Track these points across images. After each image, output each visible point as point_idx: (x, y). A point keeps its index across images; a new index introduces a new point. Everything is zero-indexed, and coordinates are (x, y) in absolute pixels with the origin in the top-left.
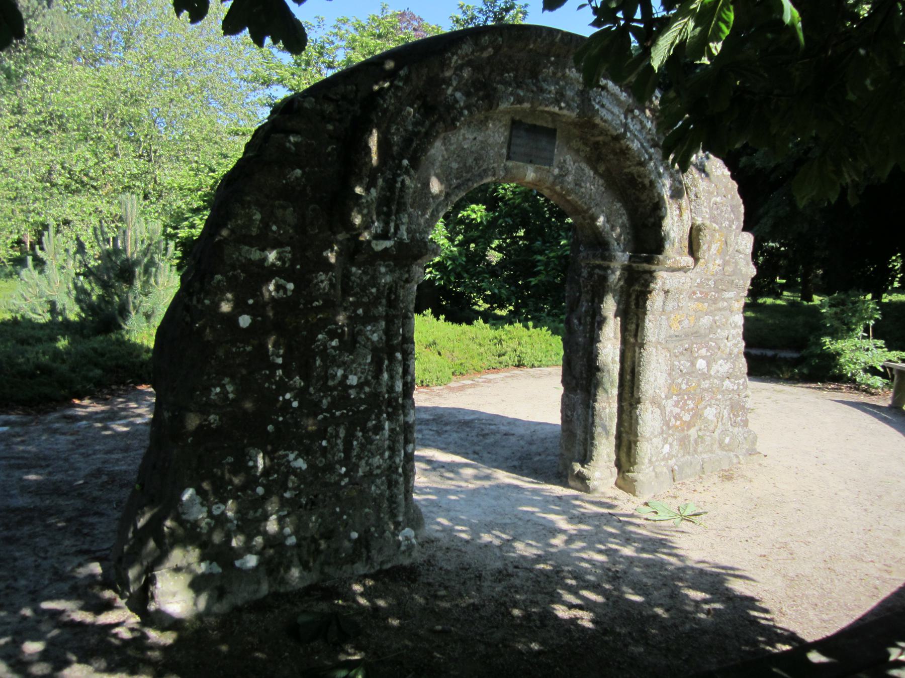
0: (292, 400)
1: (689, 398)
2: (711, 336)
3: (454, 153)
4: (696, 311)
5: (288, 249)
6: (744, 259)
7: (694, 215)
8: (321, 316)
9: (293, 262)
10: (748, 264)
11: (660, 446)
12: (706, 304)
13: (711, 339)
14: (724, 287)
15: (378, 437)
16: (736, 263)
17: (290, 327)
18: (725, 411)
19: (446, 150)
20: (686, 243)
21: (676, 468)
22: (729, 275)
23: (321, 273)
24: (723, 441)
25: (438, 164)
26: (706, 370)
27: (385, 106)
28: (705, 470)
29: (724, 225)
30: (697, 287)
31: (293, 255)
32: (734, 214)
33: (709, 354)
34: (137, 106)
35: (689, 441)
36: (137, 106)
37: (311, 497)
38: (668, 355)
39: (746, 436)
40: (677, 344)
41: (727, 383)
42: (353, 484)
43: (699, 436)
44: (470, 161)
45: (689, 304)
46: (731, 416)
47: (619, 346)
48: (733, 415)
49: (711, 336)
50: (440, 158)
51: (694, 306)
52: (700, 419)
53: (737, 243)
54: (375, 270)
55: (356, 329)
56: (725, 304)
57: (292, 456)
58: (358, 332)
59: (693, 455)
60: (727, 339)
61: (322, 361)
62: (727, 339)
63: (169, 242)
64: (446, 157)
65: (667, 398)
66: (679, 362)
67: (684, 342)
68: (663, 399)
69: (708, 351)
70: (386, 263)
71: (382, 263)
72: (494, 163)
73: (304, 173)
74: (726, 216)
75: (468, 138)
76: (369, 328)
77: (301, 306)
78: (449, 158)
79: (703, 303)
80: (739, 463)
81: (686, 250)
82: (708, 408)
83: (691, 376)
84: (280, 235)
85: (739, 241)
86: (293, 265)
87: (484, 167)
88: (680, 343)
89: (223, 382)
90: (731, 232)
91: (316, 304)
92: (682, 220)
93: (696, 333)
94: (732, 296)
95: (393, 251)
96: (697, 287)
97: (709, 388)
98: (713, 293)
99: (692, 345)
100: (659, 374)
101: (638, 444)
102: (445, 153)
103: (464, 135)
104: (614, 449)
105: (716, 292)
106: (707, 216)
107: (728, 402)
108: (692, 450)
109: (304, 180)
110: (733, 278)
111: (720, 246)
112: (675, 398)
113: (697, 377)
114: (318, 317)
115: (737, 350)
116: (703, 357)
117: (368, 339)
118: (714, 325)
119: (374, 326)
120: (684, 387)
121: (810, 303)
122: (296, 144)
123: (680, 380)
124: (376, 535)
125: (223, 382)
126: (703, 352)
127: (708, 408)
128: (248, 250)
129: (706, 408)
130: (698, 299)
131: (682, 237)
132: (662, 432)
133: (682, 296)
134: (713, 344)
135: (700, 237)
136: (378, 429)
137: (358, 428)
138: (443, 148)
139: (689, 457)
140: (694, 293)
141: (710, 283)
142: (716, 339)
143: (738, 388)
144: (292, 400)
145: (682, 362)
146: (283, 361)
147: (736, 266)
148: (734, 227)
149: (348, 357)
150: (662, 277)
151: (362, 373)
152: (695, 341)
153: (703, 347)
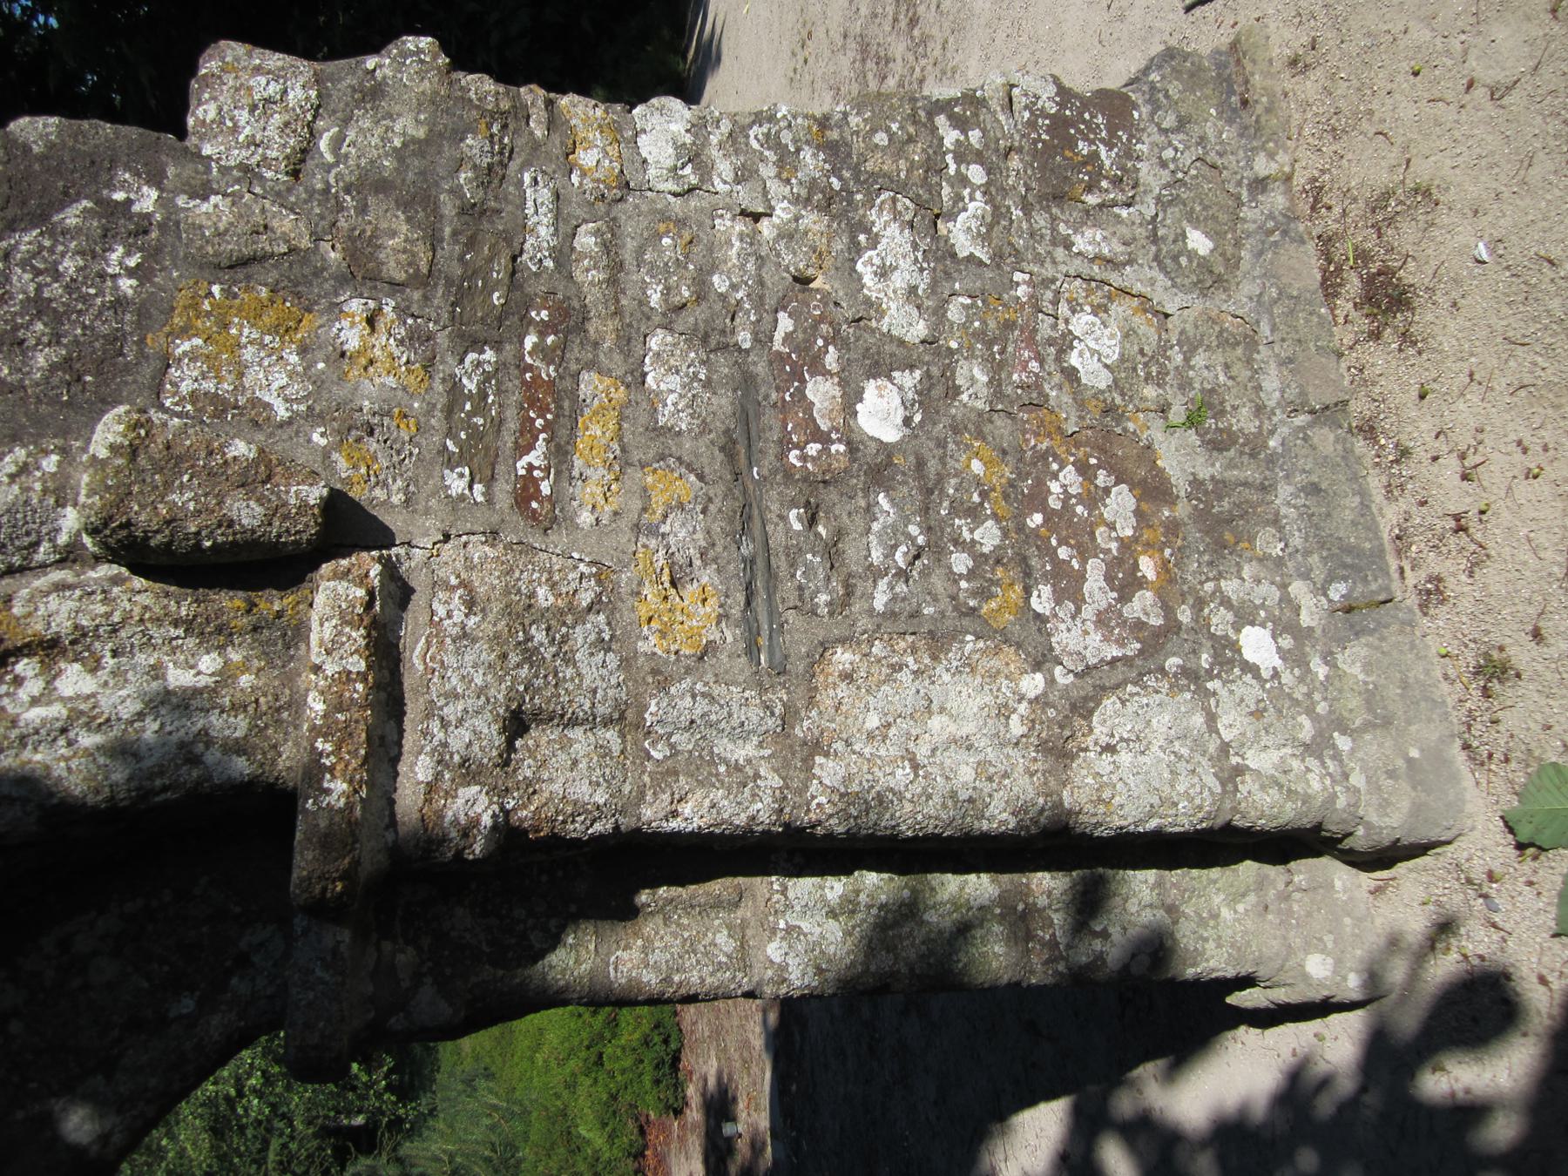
1: (1038, 499)
2: (744, 338)
4: (623, 462)
6: (346, 121)
7: (43, 553)
10: (373, 94)
11: (1249, 689)
12: (590, 384)
13: (763, 338)
14: (498, 273)
16: (369, 184)
18: (1081, 243)
20: (229, 602)
21: (1338, 591)
22: (434, 242)
24: (1204, 264)
26: (909, 380)
28: (1330, 400)
29: (127, 285)
30: (490, 481)
32: (67, 199)
33: (831, 359)
34: (145, 694)
35: (1221, 487)
36: (145, 694)
38: (843, 657)
39: (1169, 121)
40: (787, 590)
41: (962, 234)
43: (1192, 421)
45: (585, 518)
46: (1092, 200)
47: (776, 881)
48: (1089, 189)
49: (744, 338)
51: (598, 474)
52: (1120, 419)
53: (248, 172)
56: (586, 240)
59: (1272, 460)
60: (756, 217)
62: (756, 217)
63: (371, 200)
65: (1042, 660)
66: (876, 574)
67: (777, 538)
68: (1051, 682)
69: (818, 368)
74: (69, 265)
79: (578, 406)
80: (1288, 178)
81: (273, 602)
82: (1074, 359)
83: (941, 479)
85: (238, 156)
88: (780, 563)
90: (172, 223)
92: (80, 634)
93: (729, 450)
94: (545, 194)
96: (490, 481)
97: (988, 360)
98: (530, 341)
99: (788, 473)
100: (936, 723)
104: (1215, 872)
105: (526, 323)
106: (50, 463)
107: (1041, 220)
108: (1250, 473)
110: (448, 207)
111: (255, 317)
112: (1042, 601)
113: (941, 444)
115: (807, 154)
116: (851, 399)
118: (687, 320)
120: (988, 536)
121: (1393, 996)
123: (960, 562)
126: (821, 392)
127: (1074, 359)
129: (1071, 374)
130: (561, 454)
131: (189, 625)
132: (1192, 676)
133: (544, 597)
134: (785, 323)
135: (181, 547)
139: (1284, 491)
140: (526, 490)
141: (470, 385)
142: (759, 303)
143: (979, 158)
145: (877, 555)
147: (382, 186)
148: (147, 200)
150: (431, 788)
152: (769, 460)
153: (800, 394)
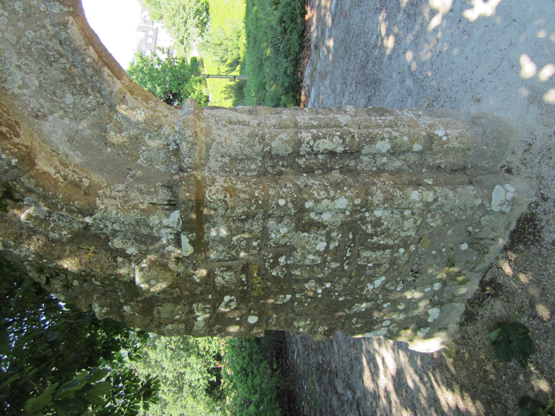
0: (324, 288)
3: (52, 100)
5: (195, 306)
8: (255, 274)
9: (205, 301)
15: (386, 223)
17: (262, 293)
19: (52, 113)
23: (216, 280)
25: (73, 124)
27: (33, 256)
31: (199, 302)
37: (411, 273)
42: (419, 242)
44: (55, 73)
50: (66, 121)
54: (213, 241)
55: (273, 245)
57: (370, 287)
58: (275, 244)
61: (296, 269)
64: (62, 112)
70: (206, 231)
71: (205, 235)
72: (44, 27)
73: (126, 304)
75: (23, 79)
76: (273, 235)
77: (245, 288)
78: (61, 108)
84: (183, 313)
86: (209, 301)
87: (58, 47)
89: (297, 326)
91: (244, 279)
95: (192, 237)
101: (550, 76)
102: (57, 115)
103: (20, 88)
109: (132, 303)
114: (256, 276)
117: (284, 236)
119: (272, 231)
122: (102, 306)
124: (477, 230)
125: (297, 326)
128: (197, 327)
136: (377, 223)
137: (369, 240)
138: (50, 118)
144: (324, 288)
146: (289, 294)
149: (298, 253)
151: (317, 239)
